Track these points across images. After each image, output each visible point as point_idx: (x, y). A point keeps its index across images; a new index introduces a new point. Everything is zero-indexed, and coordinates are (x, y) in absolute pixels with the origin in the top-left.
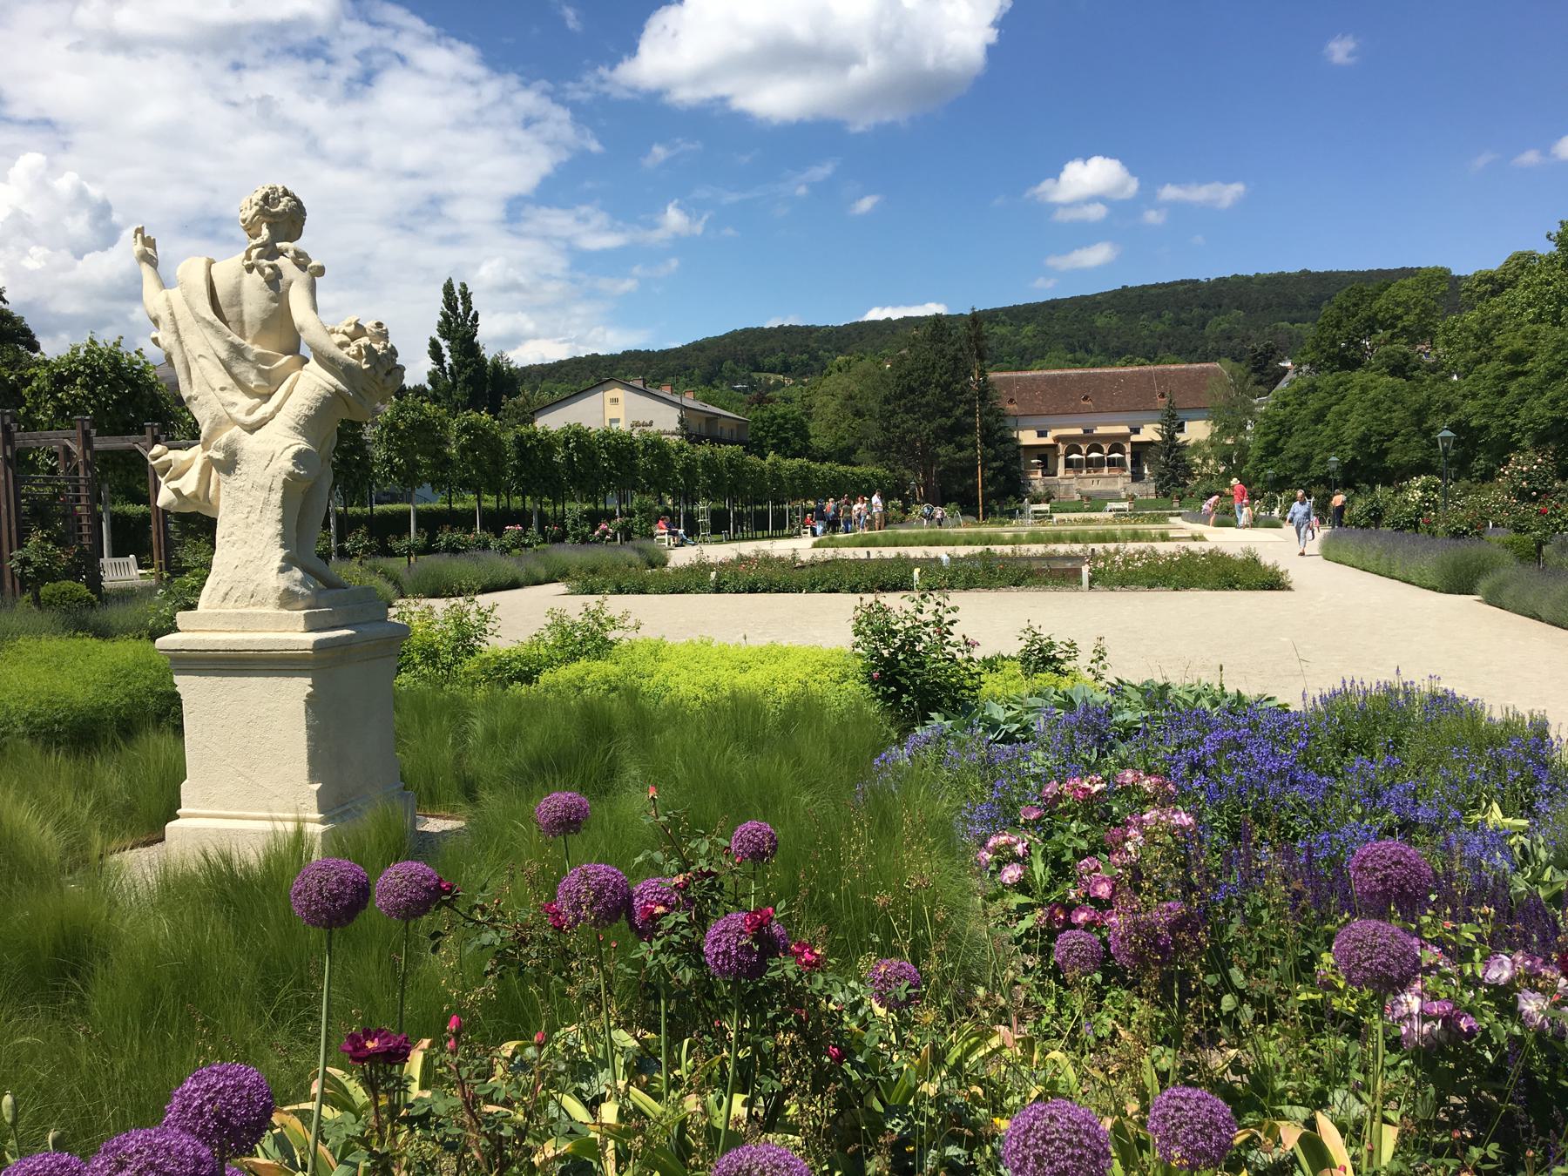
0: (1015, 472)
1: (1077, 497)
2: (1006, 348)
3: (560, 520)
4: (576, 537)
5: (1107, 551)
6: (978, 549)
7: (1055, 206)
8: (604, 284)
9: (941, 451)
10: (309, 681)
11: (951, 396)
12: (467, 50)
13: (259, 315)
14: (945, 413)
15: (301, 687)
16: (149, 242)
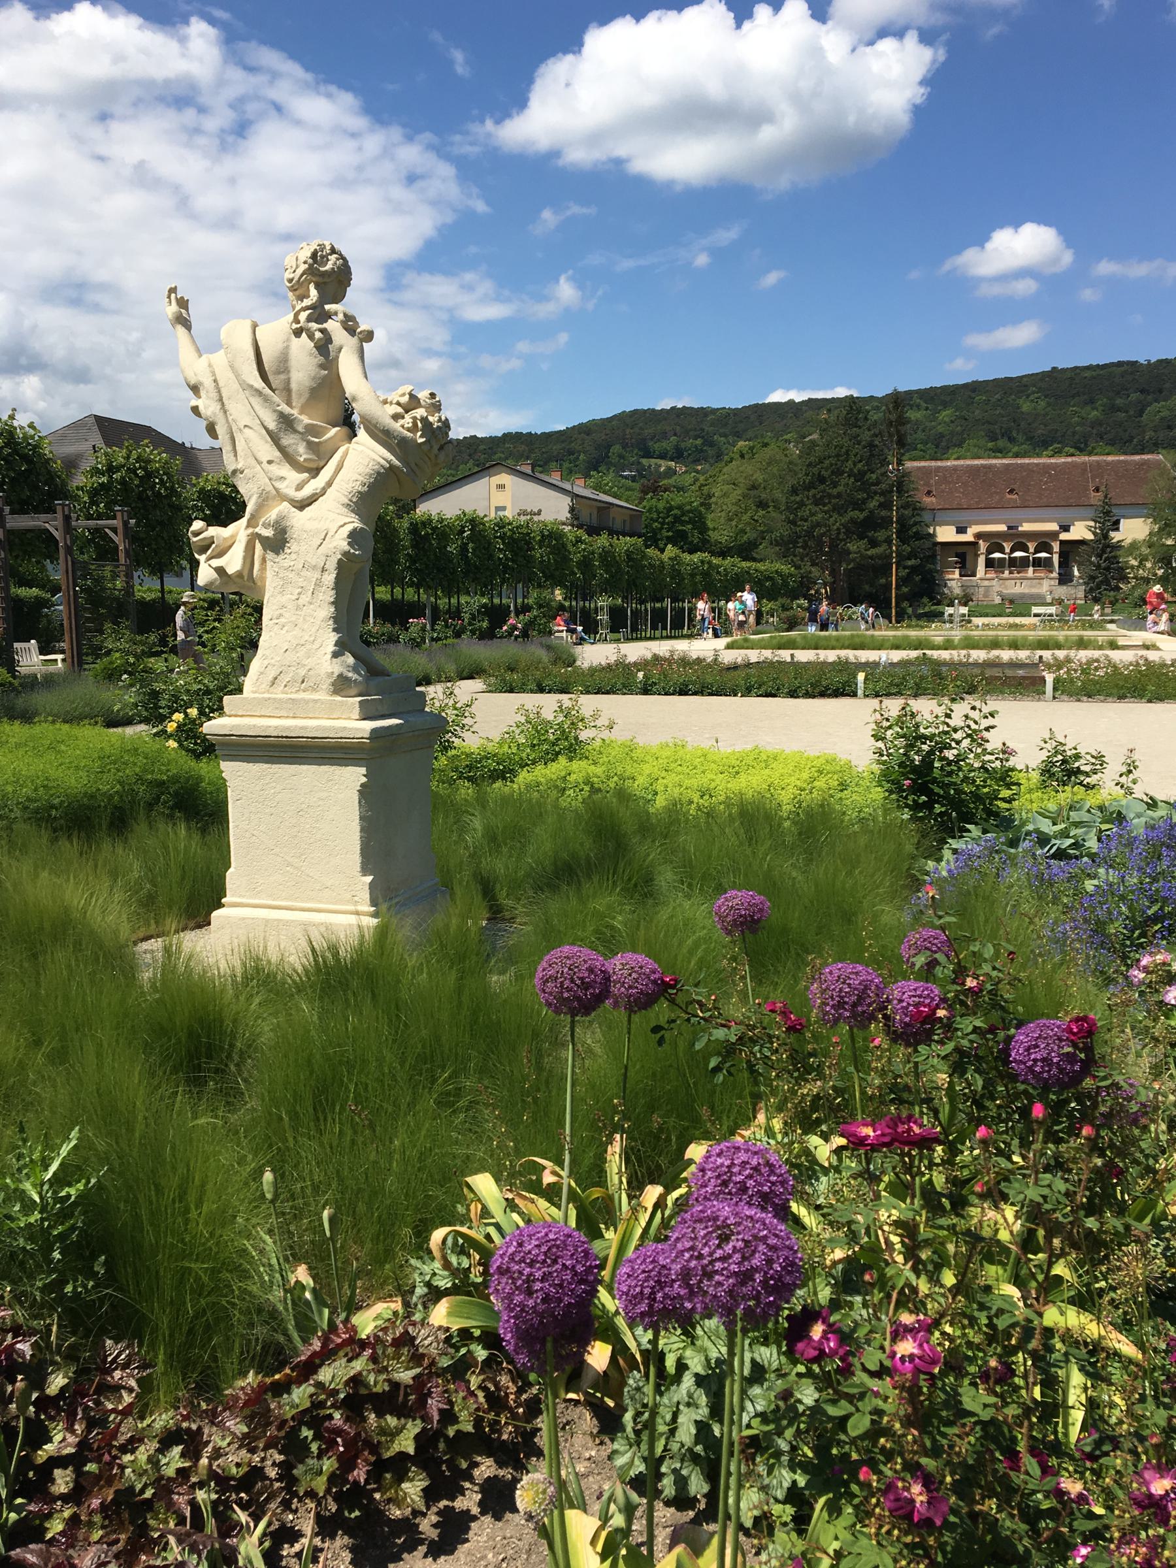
0: (931, 571)
1: (998, 600)
2: (920, 435)
3: (456, 613)
4: (473, 632)
5: (1056, 659)
6: (913, 654)
7: (981, 280)
8: (486, 361)
9: (852, 547)
10: (363, 770)
11: (865, 486)
12: (348, 99)
13: (307, 383)
14: (858, 505)
15: (354, 776)
16: (183, 303)
